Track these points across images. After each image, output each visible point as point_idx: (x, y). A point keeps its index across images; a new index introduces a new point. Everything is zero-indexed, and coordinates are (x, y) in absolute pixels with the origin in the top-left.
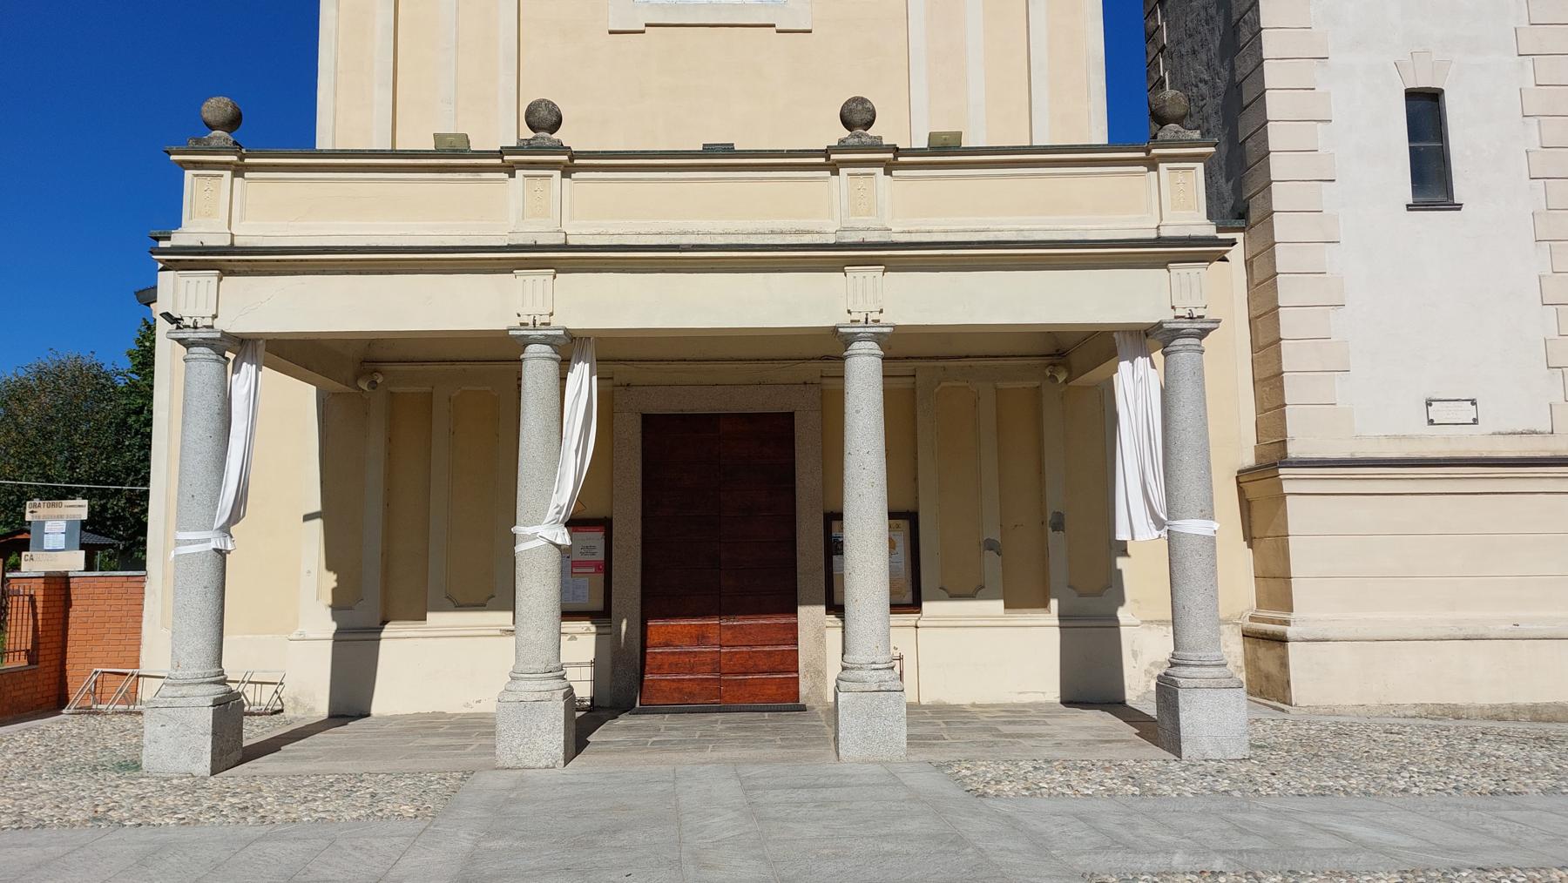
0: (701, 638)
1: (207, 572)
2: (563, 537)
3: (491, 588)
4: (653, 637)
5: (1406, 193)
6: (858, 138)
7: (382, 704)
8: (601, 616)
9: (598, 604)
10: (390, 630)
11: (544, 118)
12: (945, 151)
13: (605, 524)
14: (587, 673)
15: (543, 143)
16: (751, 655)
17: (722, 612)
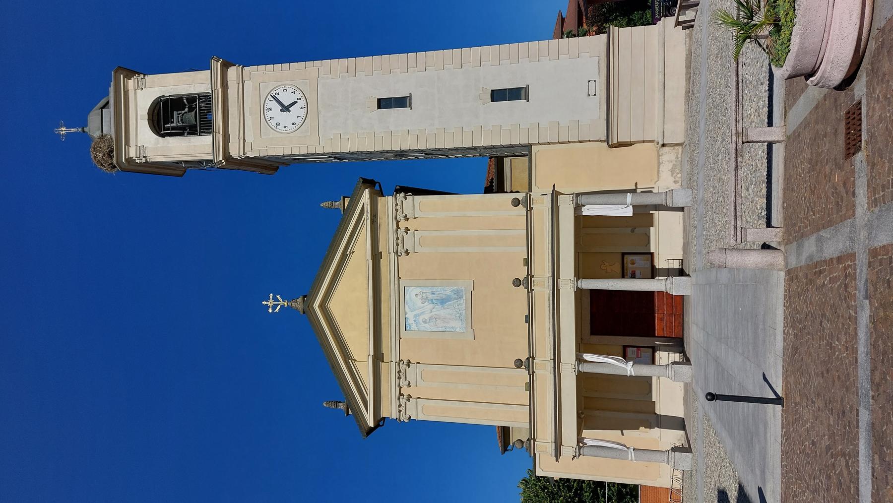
0: (662, 319)
1: (640, 453)
2: (631, 363)
3: (646, 382)
4: (661, 334)
5: (523, 101)
6: (526, 283)
7: (681, 415)
8: (654, 350)
9: (650, 350)
10: (657, 412)
11: (519, 364)
12: (528, 262)
13: (625, 348)
14: (672, 354)
15: (527, 364)
16: (667, 304)
17: (654, 313)
